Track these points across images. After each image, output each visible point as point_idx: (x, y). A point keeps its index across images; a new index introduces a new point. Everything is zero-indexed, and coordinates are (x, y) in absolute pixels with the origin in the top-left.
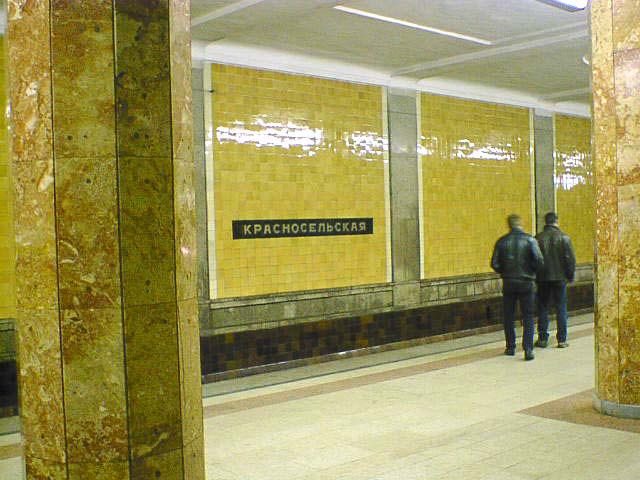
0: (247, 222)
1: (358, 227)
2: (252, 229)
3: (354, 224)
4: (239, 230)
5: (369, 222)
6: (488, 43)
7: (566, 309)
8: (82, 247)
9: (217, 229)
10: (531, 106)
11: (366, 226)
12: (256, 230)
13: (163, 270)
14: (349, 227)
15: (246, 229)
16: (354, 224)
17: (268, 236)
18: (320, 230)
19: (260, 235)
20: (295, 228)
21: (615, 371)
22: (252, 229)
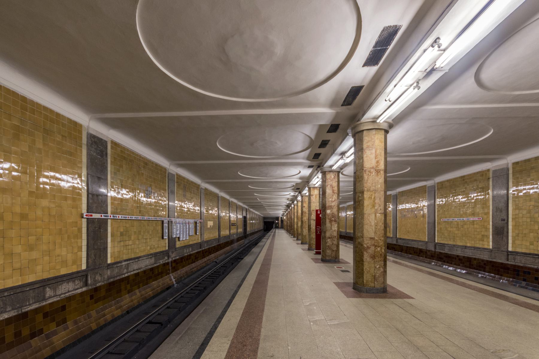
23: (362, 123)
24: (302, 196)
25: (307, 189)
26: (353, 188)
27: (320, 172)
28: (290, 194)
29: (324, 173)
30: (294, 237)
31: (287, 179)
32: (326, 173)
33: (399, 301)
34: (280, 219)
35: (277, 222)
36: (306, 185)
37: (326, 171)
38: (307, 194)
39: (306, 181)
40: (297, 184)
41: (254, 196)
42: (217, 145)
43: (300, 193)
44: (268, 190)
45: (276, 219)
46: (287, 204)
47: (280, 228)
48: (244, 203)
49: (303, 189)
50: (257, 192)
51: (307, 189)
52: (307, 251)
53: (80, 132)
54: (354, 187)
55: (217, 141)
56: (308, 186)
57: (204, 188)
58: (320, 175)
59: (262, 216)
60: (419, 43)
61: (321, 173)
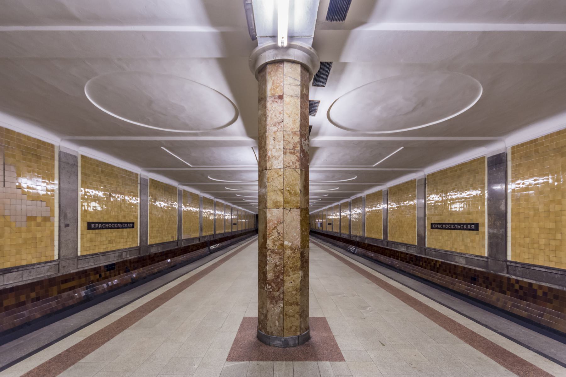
0: (93, 223)
1: (130, 226)
2: (95, 226)
3: (469, 226)
4: (90, 226)
5: (133, 223)
6: (191, 166)
7: (154, 204)
8: (278, 222)
9: (139, 255)
10: (139, 173)
11: (476, 227)
12: (436, 226)
13: (300, 354)
14: (467, 227)
15: (93, 226)
16: (129, 224)
17: (100, 229)
18: (455, 228)
19: (98, 228)
20: (110, 225)
21: (282, 167)
22: (95, 226)
44: (254, 198)
57: (203, 197)
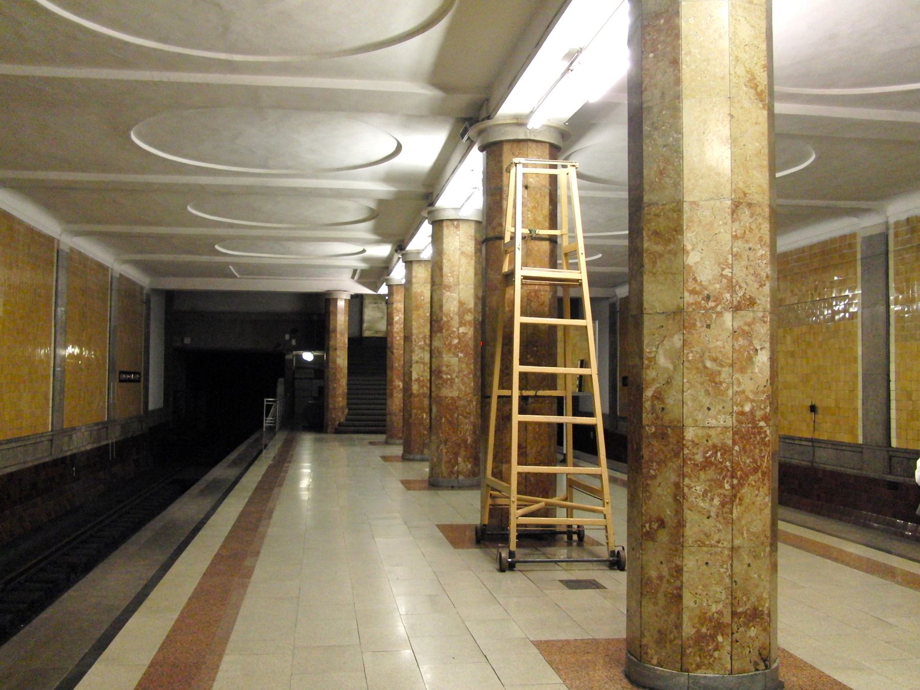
23: (498, 125)
24: (409, 264)
25: (426, 229)
26: (627, 232)
27: (475, 149)
28: (364, 251)
29: (493, 150)
30: (405, 458)
31: (334, 178)
32: (501, 150)
33: (603, 590)
34: (341, 319)
35: (308, 356)
36: (425, 214)
37: (442, 221)
38: (427, 254)
39: (384, 265)
40: (381, 202)
41: (184, 225)
42: (191, 213)
43: (400, 247)
45: (293, 333)
46: (365, 260)
47: (340, 430)
48: (105, 238)
49: (411, 231)
50: (221, 240)
51: (426, 229)
52: (425, 489)
53: (108, 271)
54: (630, 230)
55: (134, 129)
56: (429, 213)
58: (476, 159)
59: (128, 289)
60: (460, 162)
61: (482, 149)
